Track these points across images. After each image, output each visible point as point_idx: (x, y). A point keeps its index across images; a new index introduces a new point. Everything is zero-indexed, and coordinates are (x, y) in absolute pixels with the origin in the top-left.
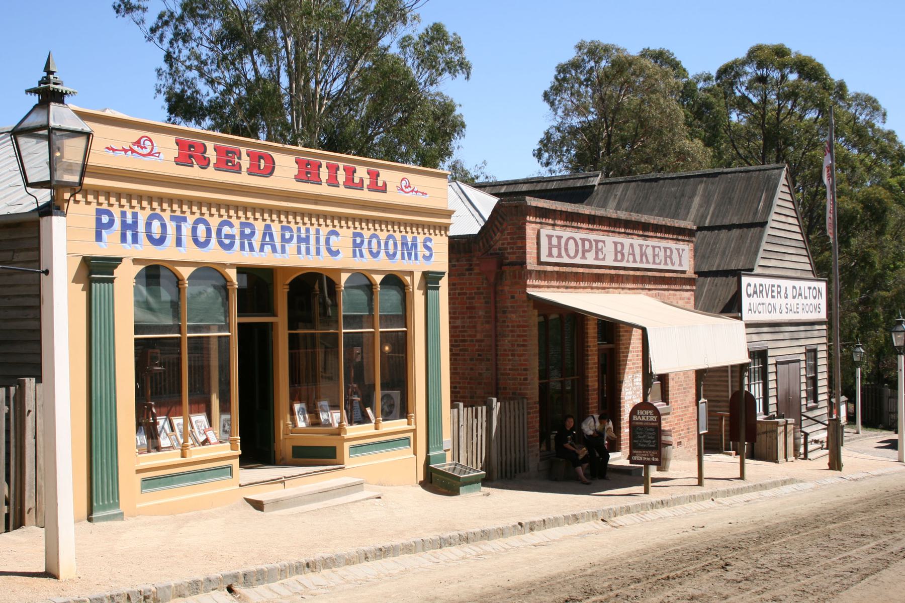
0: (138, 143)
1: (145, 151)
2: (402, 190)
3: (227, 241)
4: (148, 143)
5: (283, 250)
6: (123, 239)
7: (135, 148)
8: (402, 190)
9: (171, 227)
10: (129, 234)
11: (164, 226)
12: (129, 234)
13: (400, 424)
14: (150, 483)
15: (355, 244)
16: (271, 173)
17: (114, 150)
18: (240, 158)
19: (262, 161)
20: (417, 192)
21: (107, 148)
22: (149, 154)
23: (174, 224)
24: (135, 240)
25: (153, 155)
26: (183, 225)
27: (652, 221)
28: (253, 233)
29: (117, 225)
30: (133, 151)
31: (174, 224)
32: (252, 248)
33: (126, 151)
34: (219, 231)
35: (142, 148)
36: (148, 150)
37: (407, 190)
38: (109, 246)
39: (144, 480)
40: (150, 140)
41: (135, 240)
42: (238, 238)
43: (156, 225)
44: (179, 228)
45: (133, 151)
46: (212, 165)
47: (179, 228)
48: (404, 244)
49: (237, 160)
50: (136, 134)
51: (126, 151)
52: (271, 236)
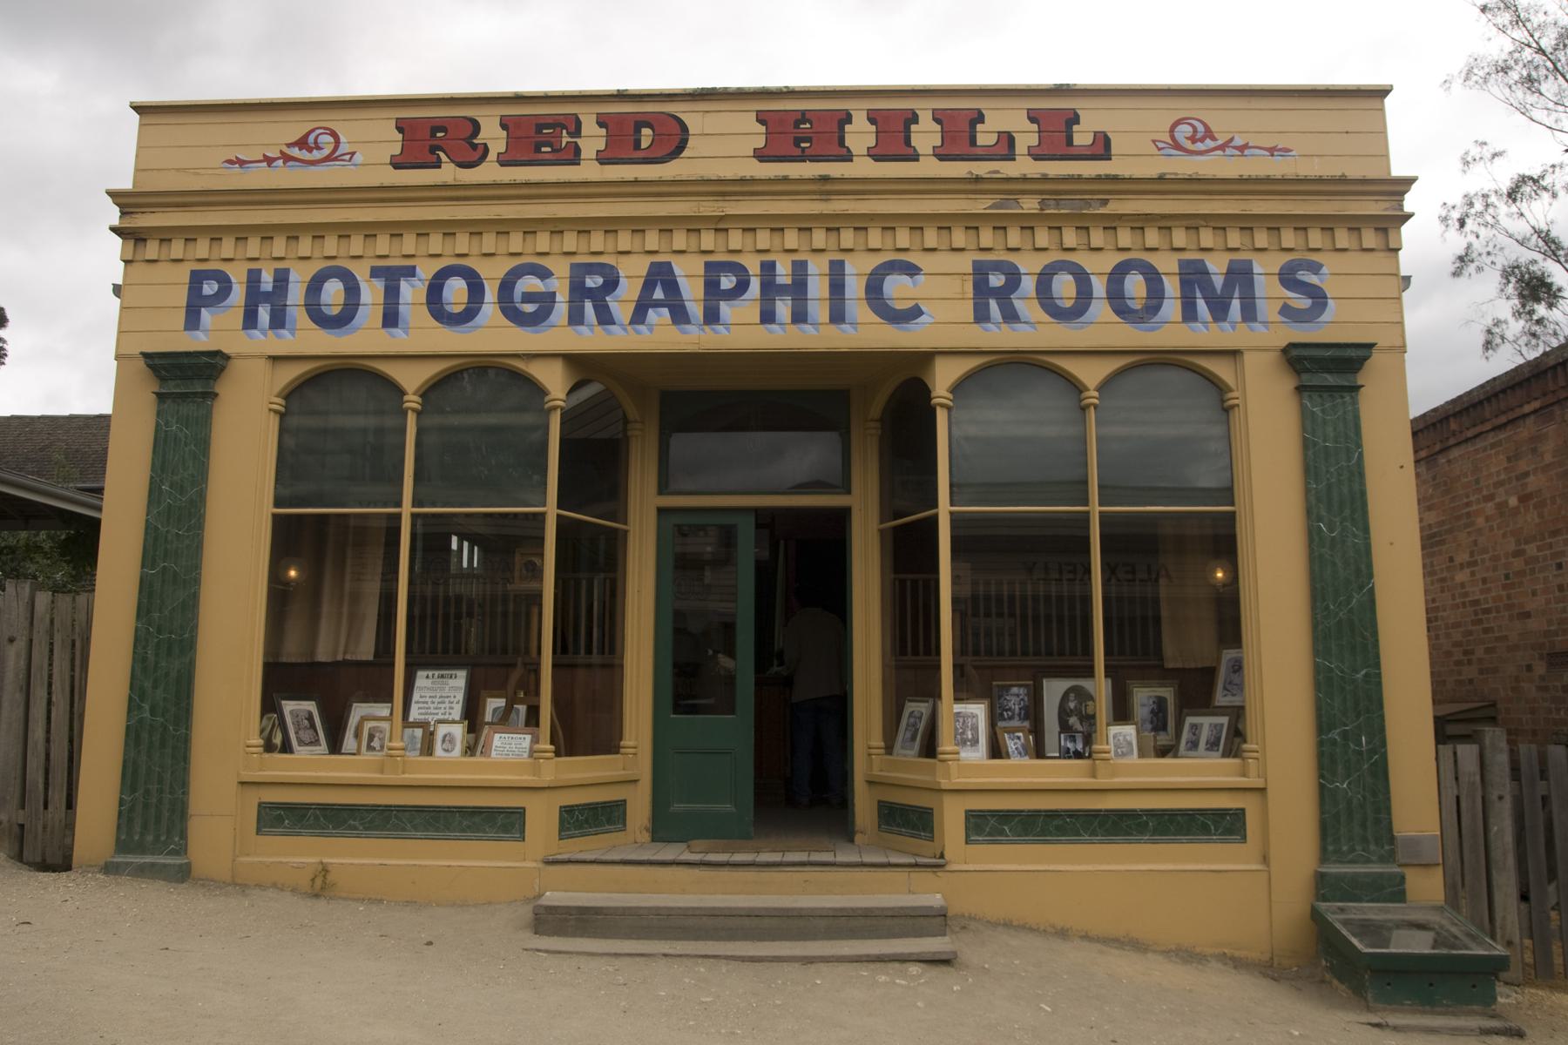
0: (302, 143)
1: (317, 155)
2: (1177, 146)
3: (529, 308)
4: (326, 139)
5: (712, 317)
6: (250, 320)
7: (295, 152)
8: (1177, 146)
9: (371, 293)
10: (264, 314)
11: (352, 289)
12: (264, 314)
13: (1197, 775)
14: (281, 817)
15: (982, 290)
16: (681, 147)
17: (241, 163)
18: (577, 132)
19: (646, 131)
20: (1242, 148)
21: (230, 162)
22: (328, 159)
23: (379, 285)
24: (278, 321)
25: (336, 159)
26: (405, 286)
27: (720, 897)
28: (611, 284)
29: (238, 294)
30: (287, 158)
31: (379, 285)
32: (605, 318)
33: (269, 161)
34: (506, 287)
35: (310, 150)
36: (326, 152)
37: (1200, 146)
38: (220, 329)
39: (262, 807)
40: (334, 134)
41: (278, 321)
42: (562, 298)
43: (333, 291)
44: (392, 293)
45: (287, 158)
46: (492, 156)
47: (392, 293)
48: (1193, 276)
49: (566, 139)
50: (294, 128)
51: (269, 161)
52: (672, 287)
